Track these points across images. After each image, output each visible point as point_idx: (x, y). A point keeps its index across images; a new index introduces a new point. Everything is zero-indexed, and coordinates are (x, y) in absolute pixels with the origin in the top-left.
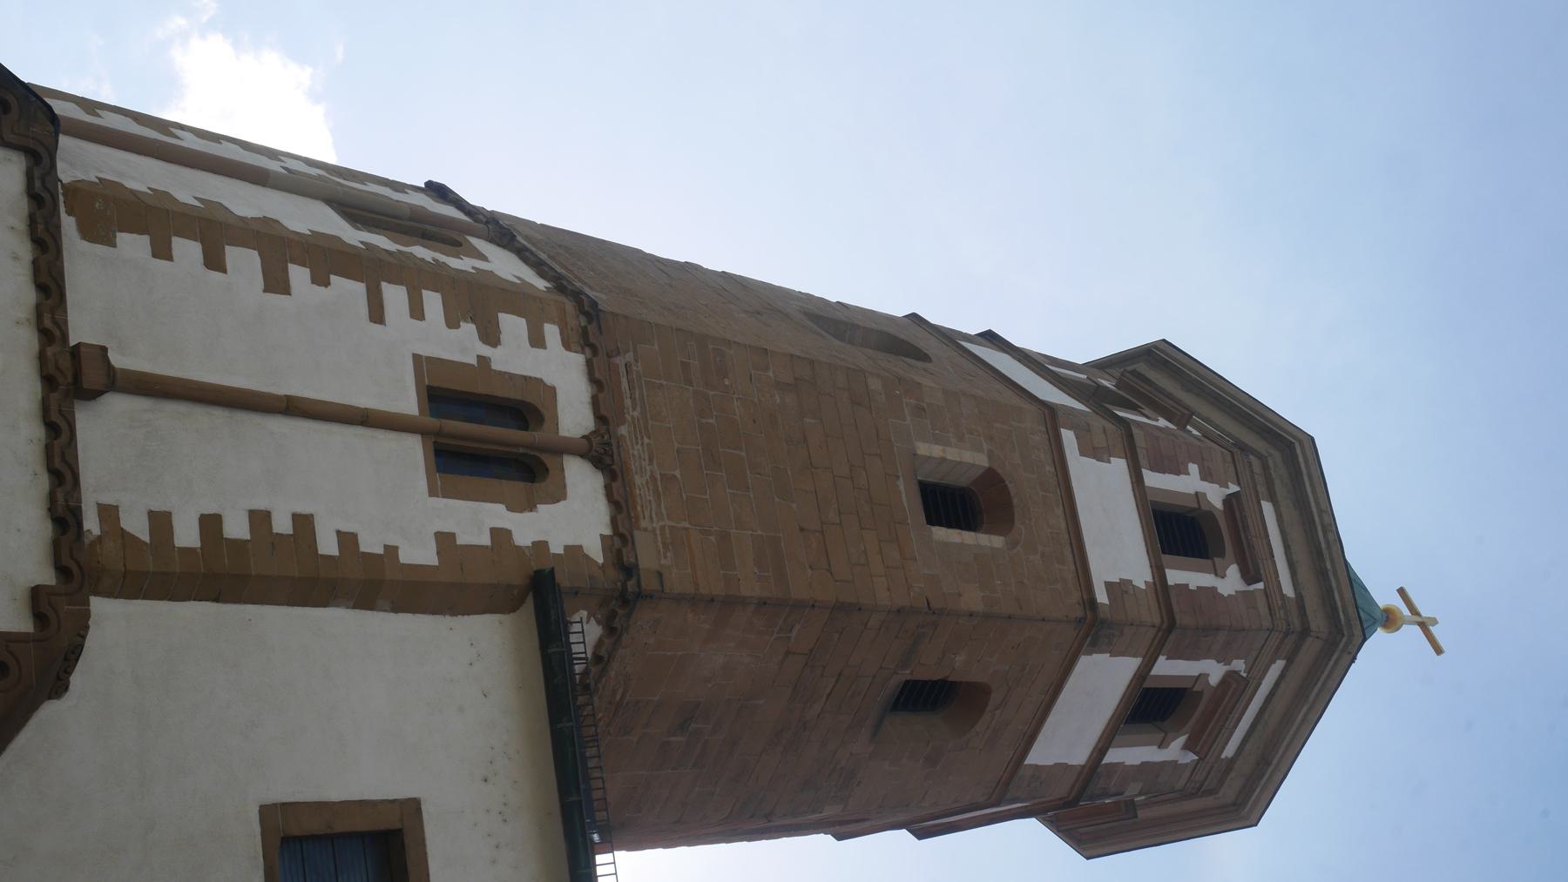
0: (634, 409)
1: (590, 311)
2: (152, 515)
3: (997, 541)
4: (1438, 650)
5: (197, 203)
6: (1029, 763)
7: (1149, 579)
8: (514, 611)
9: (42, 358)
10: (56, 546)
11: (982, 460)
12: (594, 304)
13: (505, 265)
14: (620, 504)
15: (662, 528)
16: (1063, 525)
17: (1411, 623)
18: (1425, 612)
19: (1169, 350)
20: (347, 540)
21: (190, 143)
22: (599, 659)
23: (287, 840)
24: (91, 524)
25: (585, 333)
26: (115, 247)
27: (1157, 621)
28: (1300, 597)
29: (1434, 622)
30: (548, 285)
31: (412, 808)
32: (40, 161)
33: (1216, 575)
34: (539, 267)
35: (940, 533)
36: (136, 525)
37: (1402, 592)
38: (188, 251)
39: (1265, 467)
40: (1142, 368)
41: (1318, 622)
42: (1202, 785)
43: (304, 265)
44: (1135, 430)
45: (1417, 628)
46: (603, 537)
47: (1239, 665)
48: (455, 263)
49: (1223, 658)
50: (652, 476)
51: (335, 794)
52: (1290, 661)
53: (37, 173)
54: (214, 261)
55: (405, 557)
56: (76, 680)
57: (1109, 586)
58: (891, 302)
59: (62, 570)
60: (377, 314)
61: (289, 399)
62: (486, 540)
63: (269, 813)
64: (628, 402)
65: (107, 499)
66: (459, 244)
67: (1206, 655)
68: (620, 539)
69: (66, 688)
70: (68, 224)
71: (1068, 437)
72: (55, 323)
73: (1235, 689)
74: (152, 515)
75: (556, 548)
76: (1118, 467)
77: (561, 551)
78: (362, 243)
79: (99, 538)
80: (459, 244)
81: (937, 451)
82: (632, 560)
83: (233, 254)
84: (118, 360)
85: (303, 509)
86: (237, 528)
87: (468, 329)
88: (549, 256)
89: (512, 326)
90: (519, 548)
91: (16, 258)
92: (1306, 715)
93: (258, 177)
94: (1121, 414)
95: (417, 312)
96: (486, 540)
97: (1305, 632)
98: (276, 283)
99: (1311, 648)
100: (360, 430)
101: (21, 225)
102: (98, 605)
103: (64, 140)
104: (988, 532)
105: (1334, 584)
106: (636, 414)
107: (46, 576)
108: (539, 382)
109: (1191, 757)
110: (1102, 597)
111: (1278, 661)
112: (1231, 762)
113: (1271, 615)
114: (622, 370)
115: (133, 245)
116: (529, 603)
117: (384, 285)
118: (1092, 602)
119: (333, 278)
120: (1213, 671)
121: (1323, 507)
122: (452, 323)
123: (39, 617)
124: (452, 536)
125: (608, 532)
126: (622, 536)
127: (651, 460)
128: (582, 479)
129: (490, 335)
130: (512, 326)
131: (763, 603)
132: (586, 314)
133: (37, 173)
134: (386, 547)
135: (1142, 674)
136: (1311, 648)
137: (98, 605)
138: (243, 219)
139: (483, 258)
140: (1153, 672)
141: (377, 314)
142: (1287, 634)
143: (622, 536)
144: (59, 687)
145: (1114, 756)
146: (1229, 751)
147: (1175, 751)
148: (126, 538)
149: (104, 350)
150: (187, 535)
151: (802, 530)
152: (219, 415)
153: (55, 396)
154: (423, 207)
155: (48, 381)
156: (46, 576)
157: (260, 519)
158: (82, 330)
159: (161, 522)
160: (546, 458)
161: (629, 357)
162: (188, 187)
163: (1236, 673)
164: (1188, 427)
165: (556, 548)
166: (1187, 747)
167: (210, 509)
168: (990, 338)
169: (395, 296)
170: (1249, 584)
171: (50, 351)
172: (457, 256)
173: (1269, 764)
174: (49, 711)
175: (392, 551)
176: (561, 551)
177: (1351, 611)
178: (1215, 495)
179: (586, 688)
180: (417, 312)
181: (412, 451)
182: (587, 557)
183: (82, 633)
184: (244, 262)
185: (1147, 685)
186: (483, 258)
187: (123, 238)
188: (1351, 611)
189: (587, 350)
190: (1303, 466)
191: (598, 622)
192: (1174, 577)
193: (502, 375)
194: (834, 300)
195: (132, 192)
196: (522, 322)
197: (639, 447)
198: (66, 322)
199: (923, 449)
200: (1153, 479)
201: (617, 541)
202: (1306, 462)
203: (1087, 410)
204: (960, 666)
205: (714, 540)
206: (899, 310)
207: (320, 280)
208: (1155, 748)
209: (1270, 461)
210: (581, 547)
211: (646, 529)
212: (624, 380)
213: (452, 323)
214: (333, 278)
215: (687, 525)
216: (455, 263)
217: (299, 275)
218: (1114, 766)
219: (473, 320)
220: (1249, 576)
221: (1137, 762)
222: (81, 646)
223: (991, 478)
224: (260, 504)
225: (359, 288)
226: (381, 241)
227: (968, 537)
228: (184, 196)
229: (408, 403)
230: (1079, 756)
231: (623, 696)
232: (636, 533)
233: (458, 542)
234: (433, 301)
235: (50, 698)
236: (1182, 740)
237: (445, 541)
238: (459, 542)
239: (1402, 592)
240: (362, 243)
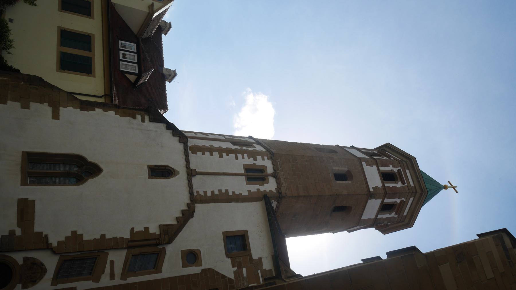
1: (272, 154)
2: (204, 192)
3: (350, 182)
4: (457, 192)
5: (209, 146)
6: (363, 218)
7: (382, 186)
8: (262, 201)
9: (187, 172)
10: (190, 197)
11: (346, 169)
12: (272, 152)
13: (259, 148)
14: (278, 183)
15: (286, 186)
16: (363, 178)
17: (450, 187)
18: (454, 185)
19: (389, 144)
20: (234, 193)
21: (210, 137)
23: (227, 237)
24: (195, 194)
25: (271, 157)
27: (384, 193)
28: (415, 186)
29: (456, 187)
30: (266, 150)
31: (246, 231)
32: (185, 143)
33: (396, 184)
34: (264, 147)
35: (338, 182)
36: (202, 193)
37: (449, 182)
38: (207, 153)
39: (407, 164)
40: (384, 148)
41: (419, 190)
42: (400, 220)
43: (225, 153)
44: (378, 160)
45: (452, 188)
47: (403, 199)
48: (250, 149)
49: (399, 198)
50: (284, 178)
51: (234, 230)
52: (414, 197)
53: (185, 146)
54: (211, 154)
55: (243, 194)
56: (194, 215)
57: (373, 188)
58: (334, 144)
59: (191, 200)
60: (237, 159)
61: (223, 173)
62: (256, 191)
63: (224, 233)
64: (279, 167)
65: (197, 190)
66: (251, 146)
67: (396, 198)
68: (278, 189)
69: (193, 217)
70: (190, 152)
71: (364, 163)
72: (188, 166)
73: (403, 204)
74: (204, 192)
75: (268, 191)
76: (374, 167)
77: (268, 191)
79: (197, 196)
80: (251, 146)
81: (337, 168)
82: (281, 192)
83: (214, 153)
84: (197, 170)
85: (226, 189)
86: (217, 192)
87: (252, 159)
88: (268, 145)
89: (259, 158)
90: (261, 191)
91: (183, 158)
92: (419, 206)
93: (219, 140)
94: (374, 157)
95: (243, 157)
96: (256, 191)
97: (416, 192)
98: (221, 156)
99: (418, 195)
100: (235, 176)
101: (183, 153)
102: (197, 205)
103: (189, 139)
104: (348, 181)
105: (421, 183)
106: (281, 169)
107: (189, 202)
108: (264, 166)
109: (397, 216)
110: (371, 190)
111: (412, 198)
112: (406, 216)
113: (409, 190)
114: (278, 162)
115: (199, 154)
116: (264, 200)
117: (238, 154)
118: (369, 191)
119: (230, 154)
120: (398, 201)
122: (249, 158)
123: (188, 207)
124: (250, 190)
125: (276, 187)
126: (279, 188)
128: (272, 180)
129: (255, 159)
130: (259, 158)
132: (271, 154)
133: (185, 146)
134: (240, 193)
136: (418, 195)
137: (197, 205)
138: (216, 147)
139: (255, 147)
140: (384, 202)
141: (237, 159)
142: (412, 193)
143: (279, 188)
144: (192, 216)
145: (379, 216)
146: (405, 214)
147: (393, 215)
148: (200, 195)
149: (195, 169)
150: (209, 194)
151: (311, 184)
152: (213, 176)
153: (189, 176)
154: (247, 140)
155: (188, 174)
156: (189, 202)
157: (220, 191)
158: (192, 167)
159: (205, 193)
160: (265, 177)
161: (279, 160)
162: (207, 144)
163: (403, 200)
164: (391, 158)
165: (268, 191)
166: (395, 214)
167: (212, 190)
168: (352, 147)
169: (240, 156)
170: (403, 185)
171: (188, 170)
172: (251, 148)
173: (413, 216)
174: (191, 220)
175: (241, 194)
176: (268, 191)
177: (425, 188)
178: (395, 170)
179: (276, 212)
180: (243, 157)
181: (243, 178)
182: (273, 192)
184: (216, 154)
185: (383, 204)
186: (255, 147)
187: (198, 153)
188: (425, 188)
189: (272, 160)
190: (414, 163)
191: (276, 202)
192: (386, 185)
193: (257, 165)
194: (322, 144)
195: (199, 146)
196: (261, 157)
198: (190, 166)
199: (334, 168)
200: (381, 168)
201: (278, 189)
202: (414, 162)
203: (368, 157)
204: (344, 203)
206: (334, 145)
207: (228, 155)
208: (389, 215)
209: (407, 162)
210: (272, 190)
211: (283, 187)
212: (279, 164)
213: (249, 158)
214: (230, 154)
215: (290, 185)
216: (250, 149)
217: (224, 155)
218: (380, 219)
219: (252, 158)
220: (403, 183)
221: (386, 217)
222: (194, 211)
223: (348, 171)
224: (220, 189)
225: (234, 155)
226: (238, 147)
227: (344, 182)
228: (207, 145)
229: (242, 171)
230: (373, 217)
231: (283, 213)
232: (281, 187)
234: (246, 156)
235: (191, 218)
236: (394, 213)
237: (249, 191)
238: (252, 191)
239: (449, 182)
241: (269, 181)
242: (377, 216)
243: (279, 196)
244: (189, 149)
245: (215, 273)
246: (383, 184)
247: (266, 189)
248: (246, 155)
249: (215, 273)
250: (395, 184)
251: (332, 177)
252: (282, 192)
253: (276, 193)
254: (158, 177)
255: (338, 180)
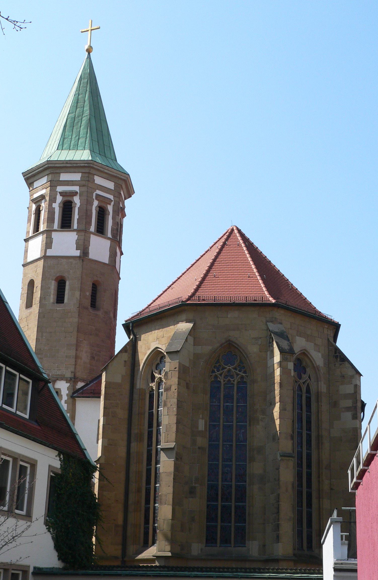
0: (47, 371)
14: (62, 378)
22: (83, 381)
26: (50, 466)
41: (87, 170)
46: (66, 383)
50: (57, 370)
68: (68, 380)
73: (98, 196)
78: (153, 556)
81: (52, 296)
118: (80, 257)
120: (96, 203)
121: (62, 163)
127: (55, 370)
131: (77, 350)
135: (94, 234)
183: (322, 569)
197: (53, 372)
205: (69, 416)
215: (64, 365)
233: (53, 204)
240: (153, 556)
241: (59, 388)
242: (109, 238)
243: (73, 380)
244: (60, 309)
245: (218, 404)
246: (74, 230)
247: (66, 394)
248: (62, 175)
249: (218, 404)
250: (76, 208)
251: (60, 307)
252: (70, 377)
253: (70, 384)
254: (32, 505)
255: (64, 300)
